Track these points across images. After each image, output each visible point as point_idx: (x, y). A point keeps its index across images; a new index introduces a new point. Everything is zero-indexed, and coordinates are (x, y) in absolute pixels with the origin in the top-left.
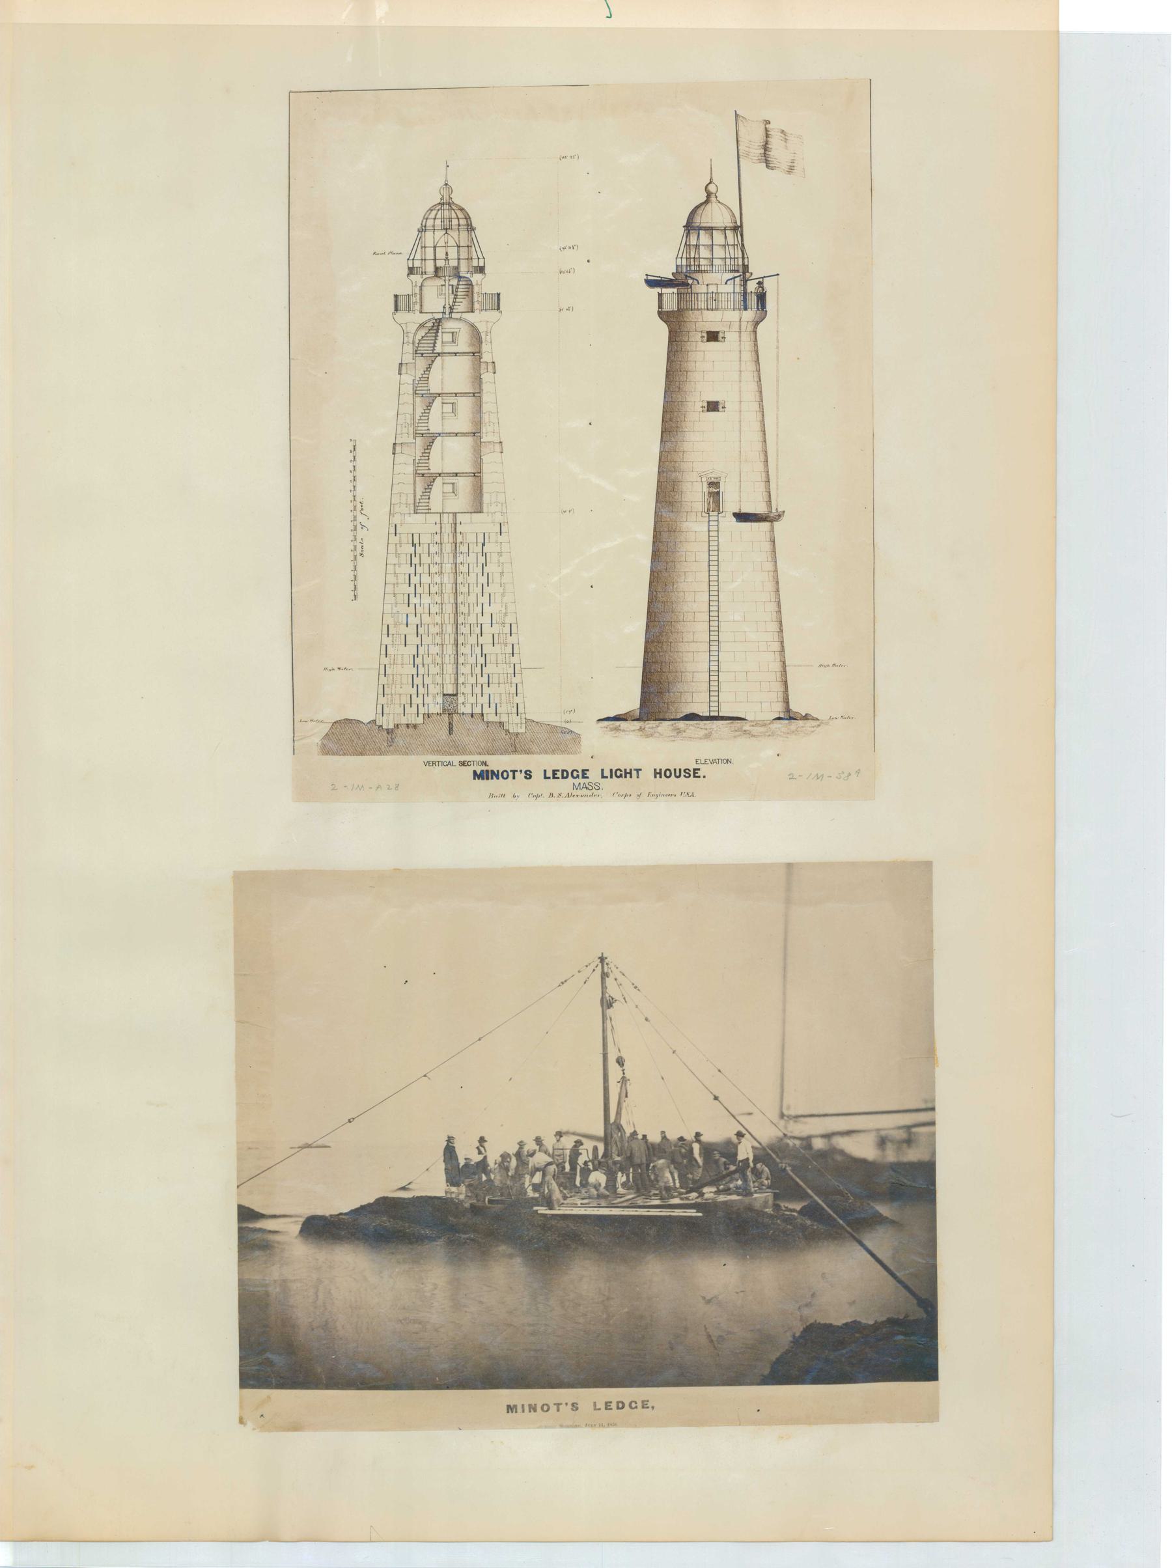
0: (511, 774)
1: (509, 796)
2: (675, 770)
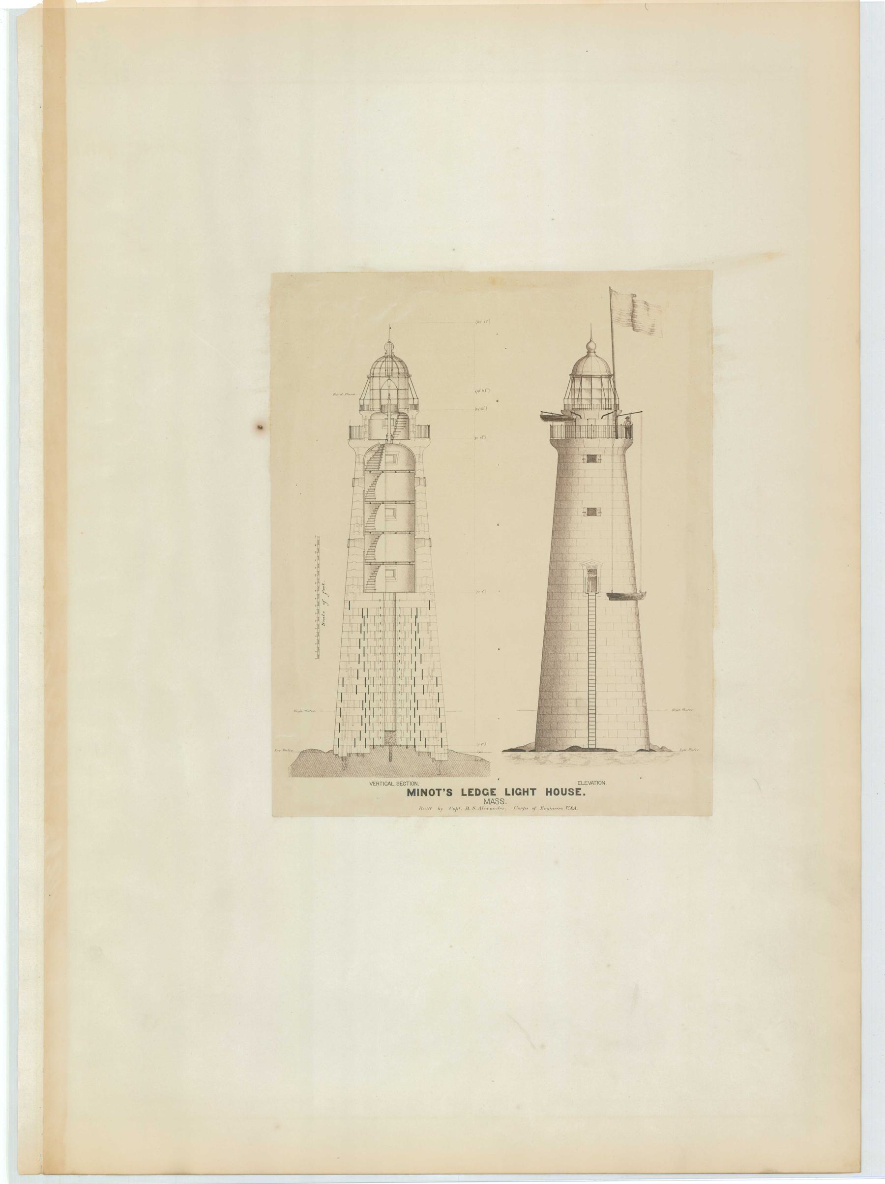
0: (436, 792)
2: (562, 789)
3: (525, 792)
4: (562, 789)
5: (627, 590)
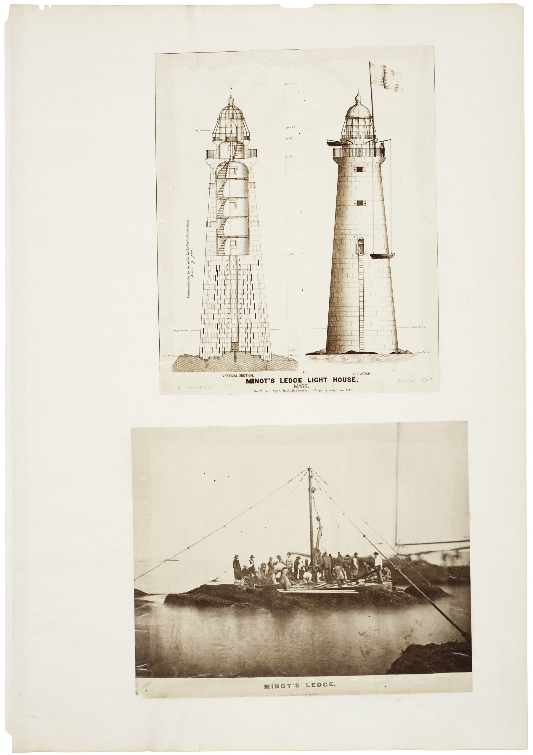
0: (265, 381)
2: (343, 378)
3: (321, 380)
4: (343, 378)
5: (383, 252)
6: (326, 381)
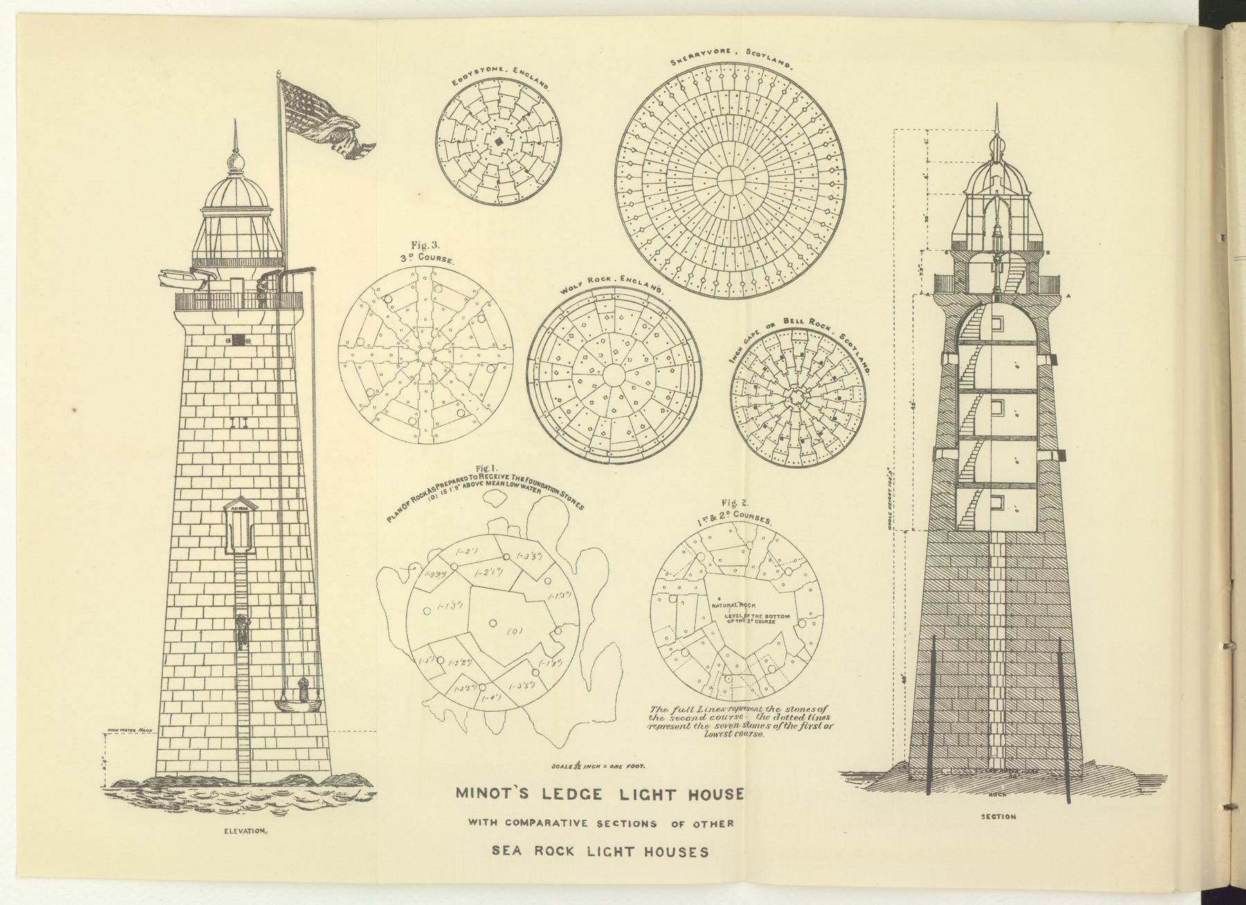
0: (503, 793)
1: (650, 286)
2: (715, 791)
4: (715, 791)
6: (506, 797)
